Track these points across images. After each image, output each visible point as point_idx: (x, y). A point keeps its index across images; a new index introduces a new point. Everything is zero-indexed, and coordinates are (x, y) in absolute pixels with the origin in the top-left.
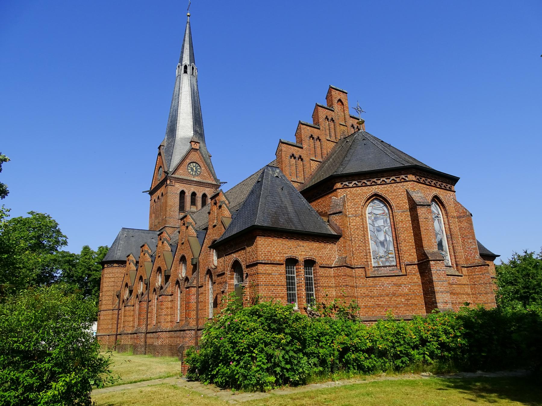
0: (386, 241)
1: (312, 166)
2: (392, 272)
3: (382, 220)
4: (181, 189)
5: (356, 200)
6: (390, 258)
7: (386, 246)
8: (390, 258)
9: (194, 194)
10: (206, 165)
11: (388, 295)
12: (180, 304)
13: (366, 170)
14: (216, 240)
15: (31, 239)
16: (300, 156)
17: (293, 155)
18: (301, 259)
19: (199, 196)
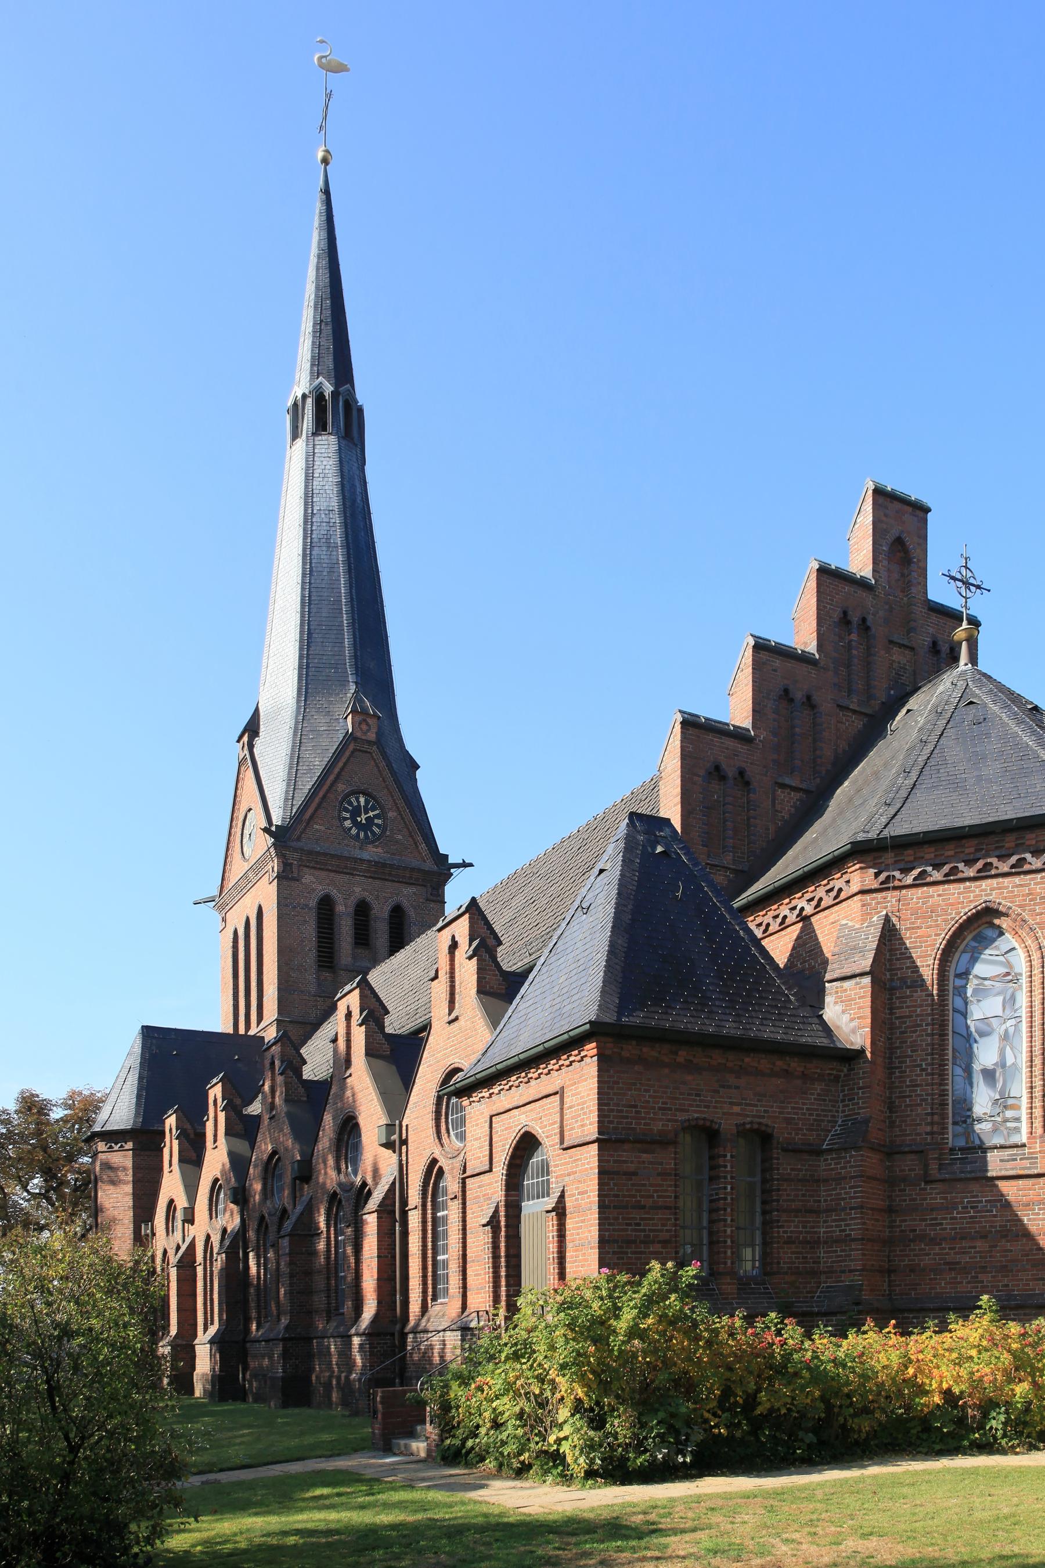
0: (1003, 1065)
1: (778, 807)
2: (1009, 1165)
3: (1000, 999)
4: (321, 890)
5: (920, 932)
6: (1006, 1120)
7: (999, 1085)
8: (1006, 1120)
9: (362, 910)
10: (401, 803)
11: (984, 1237)
12: (507, 1291)
13: (968, 822)
14: (458, 1070)
15: (732, 1263)
16: (742, 773)
17: (717, 768)
18: (727, 1126)
19: (381, 911)
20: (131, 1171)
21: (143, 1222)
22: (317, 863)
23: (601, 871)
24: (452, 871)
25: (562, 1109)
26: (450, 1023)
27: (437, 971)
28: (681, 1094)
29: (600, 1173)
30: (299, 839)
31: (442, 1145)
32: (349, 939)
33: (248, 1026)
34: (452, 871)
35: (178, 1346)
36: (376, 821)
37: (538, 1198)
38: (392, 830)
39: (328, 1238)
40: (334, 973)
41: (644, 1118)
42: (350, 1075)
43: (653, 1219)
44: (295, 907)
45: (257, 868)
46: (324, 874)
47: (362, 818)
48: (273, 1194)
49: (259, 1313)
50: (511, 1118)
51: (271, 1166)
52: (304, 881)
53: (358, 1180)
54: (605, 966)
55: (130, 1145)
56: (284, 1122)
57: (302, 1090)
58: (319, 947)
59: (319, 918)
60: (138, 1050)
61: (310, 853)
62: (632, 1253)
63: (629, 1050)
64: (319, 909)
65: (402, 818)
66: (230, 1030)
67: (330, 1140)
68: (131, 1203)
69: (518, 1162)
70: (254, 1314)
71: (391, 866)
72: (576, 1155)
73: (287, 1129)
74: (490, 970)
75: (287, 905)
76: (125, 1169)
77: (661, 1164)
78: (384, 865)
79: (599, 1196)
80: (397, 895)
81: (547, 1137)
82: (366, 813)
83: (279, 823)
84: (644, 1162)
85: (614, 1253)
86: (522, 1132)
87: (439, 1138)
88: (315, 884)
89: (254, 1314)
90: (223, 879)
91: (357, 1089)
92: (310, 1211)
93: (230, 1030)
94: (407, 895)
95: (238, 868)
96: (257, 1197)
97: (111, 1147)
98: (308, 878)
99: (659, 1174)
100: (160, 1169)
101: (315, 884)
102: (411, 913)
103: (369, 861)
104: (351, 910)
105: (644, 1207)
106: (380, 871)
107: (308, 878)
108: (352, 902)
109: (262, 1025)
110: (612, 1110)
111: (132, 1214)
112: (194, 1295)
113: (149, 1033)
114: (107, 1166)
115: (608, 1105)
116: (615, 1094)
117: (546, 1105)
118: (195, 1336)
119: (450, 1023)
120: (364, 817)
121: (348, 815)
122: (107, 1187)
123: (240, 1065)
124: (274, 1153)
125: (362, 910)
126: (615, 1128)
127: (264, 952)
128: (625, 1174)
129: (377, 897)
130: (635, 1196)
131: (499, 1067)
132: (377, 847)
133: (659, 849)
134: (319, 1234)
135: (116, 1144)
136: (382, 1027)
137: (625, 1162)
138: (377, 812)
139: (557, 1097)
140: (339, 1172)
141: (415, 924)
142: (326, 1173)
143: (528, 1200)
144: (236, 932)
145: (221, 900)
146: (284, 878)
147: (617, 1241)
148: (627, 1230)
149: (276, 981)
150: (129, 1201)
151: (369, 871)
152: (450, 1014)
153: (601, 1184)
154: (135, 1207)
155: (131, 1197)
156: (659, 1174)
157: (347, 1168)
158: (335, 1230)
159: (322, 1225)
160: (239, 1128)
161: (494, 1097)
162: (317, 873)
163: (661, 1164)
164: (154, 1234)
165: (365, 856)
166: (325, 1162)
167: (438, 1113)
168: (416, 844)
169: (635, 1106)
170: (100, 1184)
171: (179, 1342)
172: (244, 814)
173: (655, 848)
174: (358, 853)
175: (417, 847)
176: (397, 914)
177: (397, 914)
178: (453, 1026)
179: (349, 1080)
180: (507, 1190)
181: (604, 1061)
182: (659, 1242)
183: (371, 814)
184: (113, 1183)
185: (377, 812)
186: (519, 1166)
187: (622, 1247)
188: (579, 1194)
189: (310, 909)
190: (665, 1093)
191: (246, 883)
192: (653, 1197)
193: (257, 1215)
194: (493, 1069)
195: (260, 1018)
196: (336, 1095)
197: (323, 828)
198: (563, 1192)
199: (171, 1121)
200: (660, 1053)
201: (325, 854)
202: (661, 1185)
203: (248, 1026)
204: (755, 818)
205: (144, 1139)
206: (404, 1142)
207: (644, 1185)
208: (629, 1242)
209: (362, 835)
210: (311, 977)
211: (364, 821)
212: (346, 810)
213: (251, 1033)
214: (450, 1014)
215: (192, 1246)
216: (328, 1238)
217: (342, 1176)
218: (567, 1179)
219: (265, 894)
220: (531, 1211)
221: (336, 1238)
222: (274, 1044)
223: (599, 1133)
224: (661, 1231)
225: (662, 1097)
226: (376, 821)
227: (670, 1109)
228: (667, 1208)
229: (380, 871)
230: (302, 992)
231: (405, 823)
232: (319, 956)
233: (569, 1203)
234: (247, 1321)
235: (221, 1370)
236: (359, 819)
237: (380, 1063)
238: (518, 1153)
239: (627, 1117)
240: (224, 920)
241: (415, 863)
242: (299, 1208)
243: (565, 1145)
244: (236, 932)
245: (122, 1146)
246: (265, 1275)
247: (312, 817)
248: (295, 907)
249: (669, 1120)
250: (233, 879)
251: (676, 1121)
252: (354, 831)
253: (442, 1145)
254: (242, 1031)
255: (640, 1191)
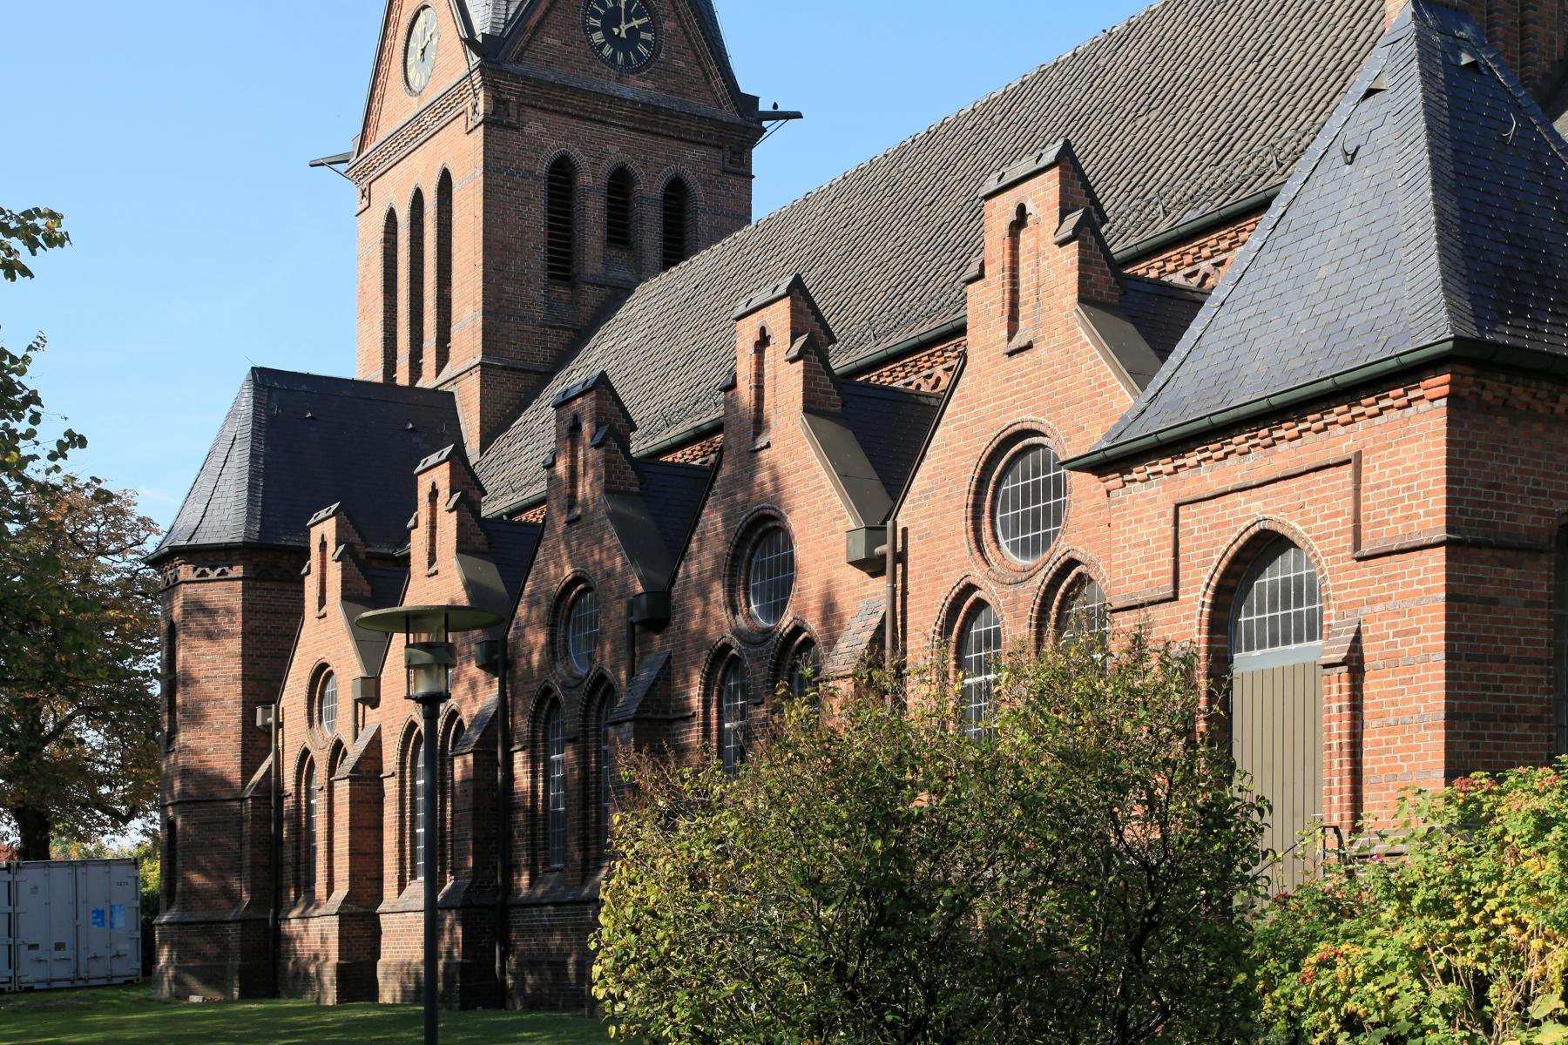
9: (620, 183)
19: (650, 187)
20: (239, 616)
21: (259, 703)
22: (548, 100)
23: (1370, 92)
24: (765, 124)
25: (1357, 490)
26: (1011, 354)
27: (982, 266)
28: (1560, 468)
29: (1448, 598)
30: (519, 59)
31: (987, 562)
32: (599, 232)
33: (416, 370)
34: (765, 124)
35: (351, 915)
36: (643, 35)
37: (1274, 643)
38: (669, 51)
39: (706, 725)
40: (573, 287)
41: (1509, 507)
42: (768, 446)
43: (1517, 680)
44: (512, 175)
45: (443, 107)
46: (560, 120)
47: (622, 30)
48: (567, 653)
49: (533, 856)
50: (1224, 508)
51: (565, 608)
52: (527, 130)
53: (786, 622)
54: (1438, 247)
55: (238, 571)
56: (603, 529)
57: (631, 474)
58: (550, 243)
59: (550, 195)
60: (247, 407)
61: (539, 83)
62: (1491, 737)
63: (1494, 389)
64: (550, 179)
65: (686, 33)
66: (378, 377)
67: (717, 556)
68: (238, 671)
69: (1231, 583)
70: (523, 858)
71: (669, 112)
72: (1394, 568)
73: (611, 539)
74: (1097, 264)
75: (498, 171)
76: (229, 611)
77: (1531, 586)
78: (657, 110)
79: (1447, 637)
80: (677, 160)
81: (1317, 538)
82: (628, 21)
83: (487, 31)
84: (1507, 582)
85: (1466, 736)
86: (1252, 531)
87: (981, 551)
88: (547, 137)
89: (523, 858)
90: (366, 125)
91: (784, 465)
92: (667, 675)
93: (378, 377)
94: (693, 162)
95: (397, 110)
96: (536, 658)
97: (203, 574)
98: (534, 126)
99: (1528, 604)
100: (298, 613)
101: (547, 137)
102: (698, 191)
103: (633, 102)
104: (603, 182)
105: (1506, 659)
106: (650, 120)
107: (534, 126)
108: (605, 169)
109: (447, 372)
110: (1465, 492)
111: (240, 690)
112: (379, 828)
113: (266, 381)
114: (197, 608)
115: (1460, 482)
116: (1469, 463)
117: (1314, 483)
118: (379, 897)
119: (1011, 354)
120: (624, 27)
121: (598, 23)
122: (196, 643)
123: (415, 439)
124: (576, 581)
125: (620, 183)
126: (1469, 522)
127: (454, 249)
128: (1483, 601)
129: (645, 162)
130: (1494, 640)
131: (1215, 419)
132: (645, 79)
133: (1466, 59)
134: (688, 719)
135: (213, 568)
136: (825, 360)
137: (1481, 580)
138: (645, 20)
139: (1348, 470)
140: (735, 612)
141: (704, 211)
142: (705, 614)
143: (1249, 648)
144: (391, 216)
145: (359, 165)
146: (496, 123)
147: (1468, 716)
148: (1483, 697)
149: (479, 298)
150: (235, 667)
151: (632, 119)
152: (1010, 339)
153: (1449, 618)
154: (246, 678)
155: (239, 660)
156: (1528, 604)
157: (748, 604)
158: (719, 712)
159: (696, 701)
160: (479, 540)
161: (1182, 473)
162: (548, 118)
163: (1531, 586)
164: (280, 725)
165: (627, 92)
166: (704, 593)
167: (977, 508)
168: (706, 76)
169: (1496, 486)
170: (181, 636)
171: (353, 908)
172: (411, 14)
173: (1459, 59)
174: (613, 88)
175: (709, 82)
176: (676, 190)
177: (676, 190)
178: (1016, 358)
179: (764, 454)
180: (1211, 632)
181: (1456, 403)
182: (1526, 720)
183: (635, 23)
184: (210, 636)
185: (645, 20)
186: (1232, 590)
187: (1477, 727)
188: (1396, 634)
189: (536, 178)
190: (1538, 465)
191: (415, 133)
192: (1517, 641)
193: (535, 687)
194: (1205, 422)
195: (442, 358)
196: (733, 481)
197: (557, 43)
198: (1358, 631)
199: (324, 529)
200: (1534, 396)
201: (564, 87)
202: (1529, 623)
203: (416, 370)
204: (1535, 23)
205: (270, 563)
206: (901, 557)
207: (1507, 621)
208: (1487, 718)
209: (620, 57)
210: (536, 292)
211: (623, 35)
212: (596, 15)
213: (427, 381)
214: (1010, 339)
215: (376, 743)
216: (706, 725)
217: (740, 619)
218: (1366, 610)
219: (461, 150)
220: (1257, 667)
221: (720, 724)
222: (582, 394)
223: (1449, 530)
224: (1529, 700)
225: (1533, 473)
226: (643, 35)
227: (1544, 493)
228: (1538, 662)
229: (650, 120)
230: (523, 318)
231: (689, 40)
232: (550, 259)
233: (1369, 650)
234: (510, 869)
235: (464, 956)
236: (616, 31)
237: (825, 424)
238: (1236, 568)
239: (1485, 504)
240: (366, 194)
241: (707, 109)
242: (644, 675)
243: (1365, 550)
244: (391, 216)
245: (223, 572)
246: (546, 791)
247: (540, 23)
248: (512, 175)
249: (1541, 512)
250: (387, 125)
251: (1552, 513)
252: (608, 51)
253: (987, 562)
254: (402, 378)
255: (1501, 631)
